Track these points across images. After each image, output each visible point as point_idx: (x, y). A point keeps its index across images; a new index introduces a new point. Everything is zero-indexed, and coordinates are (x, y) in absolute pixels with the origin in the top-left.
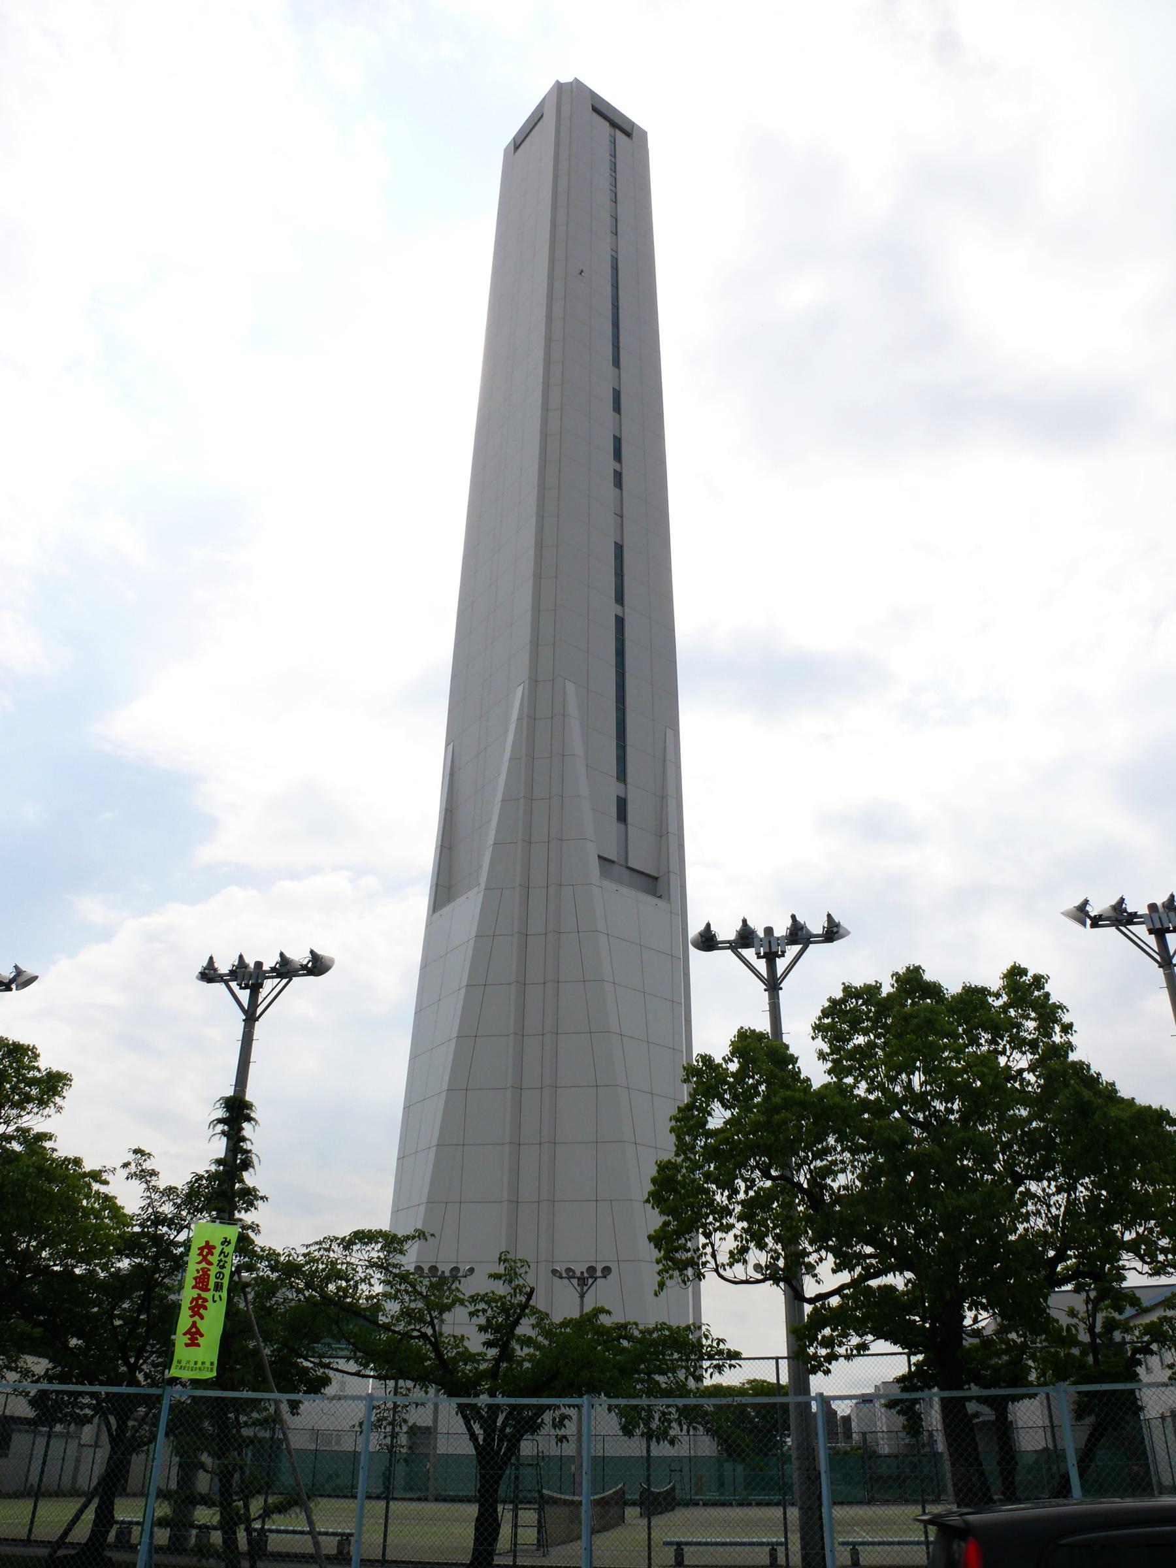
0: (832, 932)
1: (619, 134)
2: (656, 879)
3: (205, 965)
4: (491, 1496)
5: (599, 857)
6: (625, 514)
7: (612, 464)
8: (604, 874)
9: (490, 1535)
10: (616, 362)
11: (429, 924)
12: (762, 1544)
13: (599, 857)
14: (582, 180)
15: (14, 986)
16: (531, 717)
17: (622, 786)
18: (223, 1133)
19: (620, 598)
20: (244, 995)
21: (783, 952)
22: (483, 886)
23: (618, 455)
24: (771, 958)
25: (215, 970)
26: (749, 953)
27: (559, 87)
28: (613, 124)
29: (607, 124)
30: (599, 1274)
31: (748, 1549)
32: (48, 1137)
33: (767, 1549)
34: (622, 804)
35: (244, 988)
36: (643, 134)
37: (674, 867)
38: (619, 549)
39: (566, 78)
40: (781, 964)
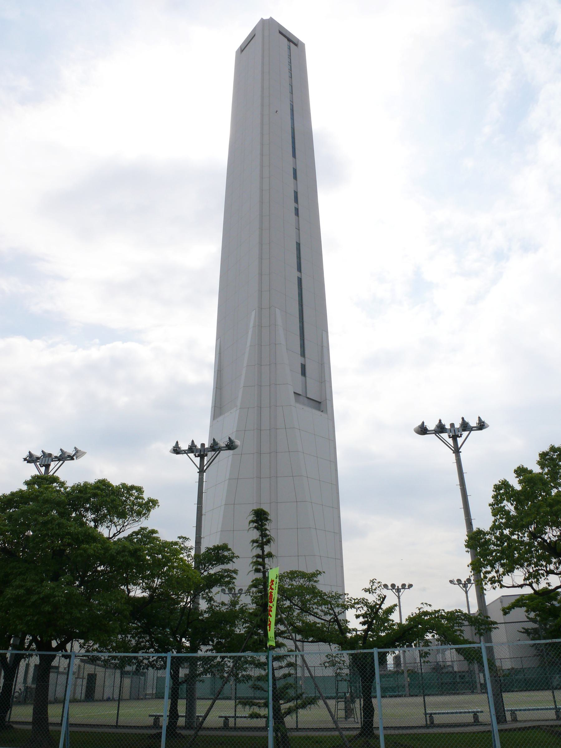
0: (481, 426)
1: (292, 44)
2: (320, 403)
3: (174, 445)
4: (368, 696)
5: (294, 393)
6: (300, 229)
7: (293, 205)
8: (297, 401)
9: (370, 714)
10: (294, 156)
11: (211, 426)
12: (469, 712)
13: (294, 393)
14: (273, 66)
15: (75, 457)
16: (260, 326)
17: (303, 358)
18: (255, 527)
19: (299, 269)
20: (197, 460)
21: (461, 435)
22: (239, 407)
23: (296, 200)
24: (455, 438)
25: (179, 448)
26: (445, 436)
27: (263, 21)
28: (289, 40)
29: (286, 40)
30: (407, 587)
31: (544, 711)
32: (153, 532)
33: (472, 715)
34: (303, 367)
35: (198, 457)
36: (303, 45)
37: (328, 397)
38: (298, 245)
39: (266, 17)
40: (460, 441)
